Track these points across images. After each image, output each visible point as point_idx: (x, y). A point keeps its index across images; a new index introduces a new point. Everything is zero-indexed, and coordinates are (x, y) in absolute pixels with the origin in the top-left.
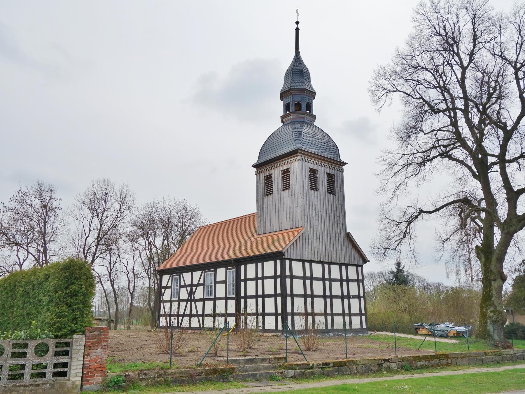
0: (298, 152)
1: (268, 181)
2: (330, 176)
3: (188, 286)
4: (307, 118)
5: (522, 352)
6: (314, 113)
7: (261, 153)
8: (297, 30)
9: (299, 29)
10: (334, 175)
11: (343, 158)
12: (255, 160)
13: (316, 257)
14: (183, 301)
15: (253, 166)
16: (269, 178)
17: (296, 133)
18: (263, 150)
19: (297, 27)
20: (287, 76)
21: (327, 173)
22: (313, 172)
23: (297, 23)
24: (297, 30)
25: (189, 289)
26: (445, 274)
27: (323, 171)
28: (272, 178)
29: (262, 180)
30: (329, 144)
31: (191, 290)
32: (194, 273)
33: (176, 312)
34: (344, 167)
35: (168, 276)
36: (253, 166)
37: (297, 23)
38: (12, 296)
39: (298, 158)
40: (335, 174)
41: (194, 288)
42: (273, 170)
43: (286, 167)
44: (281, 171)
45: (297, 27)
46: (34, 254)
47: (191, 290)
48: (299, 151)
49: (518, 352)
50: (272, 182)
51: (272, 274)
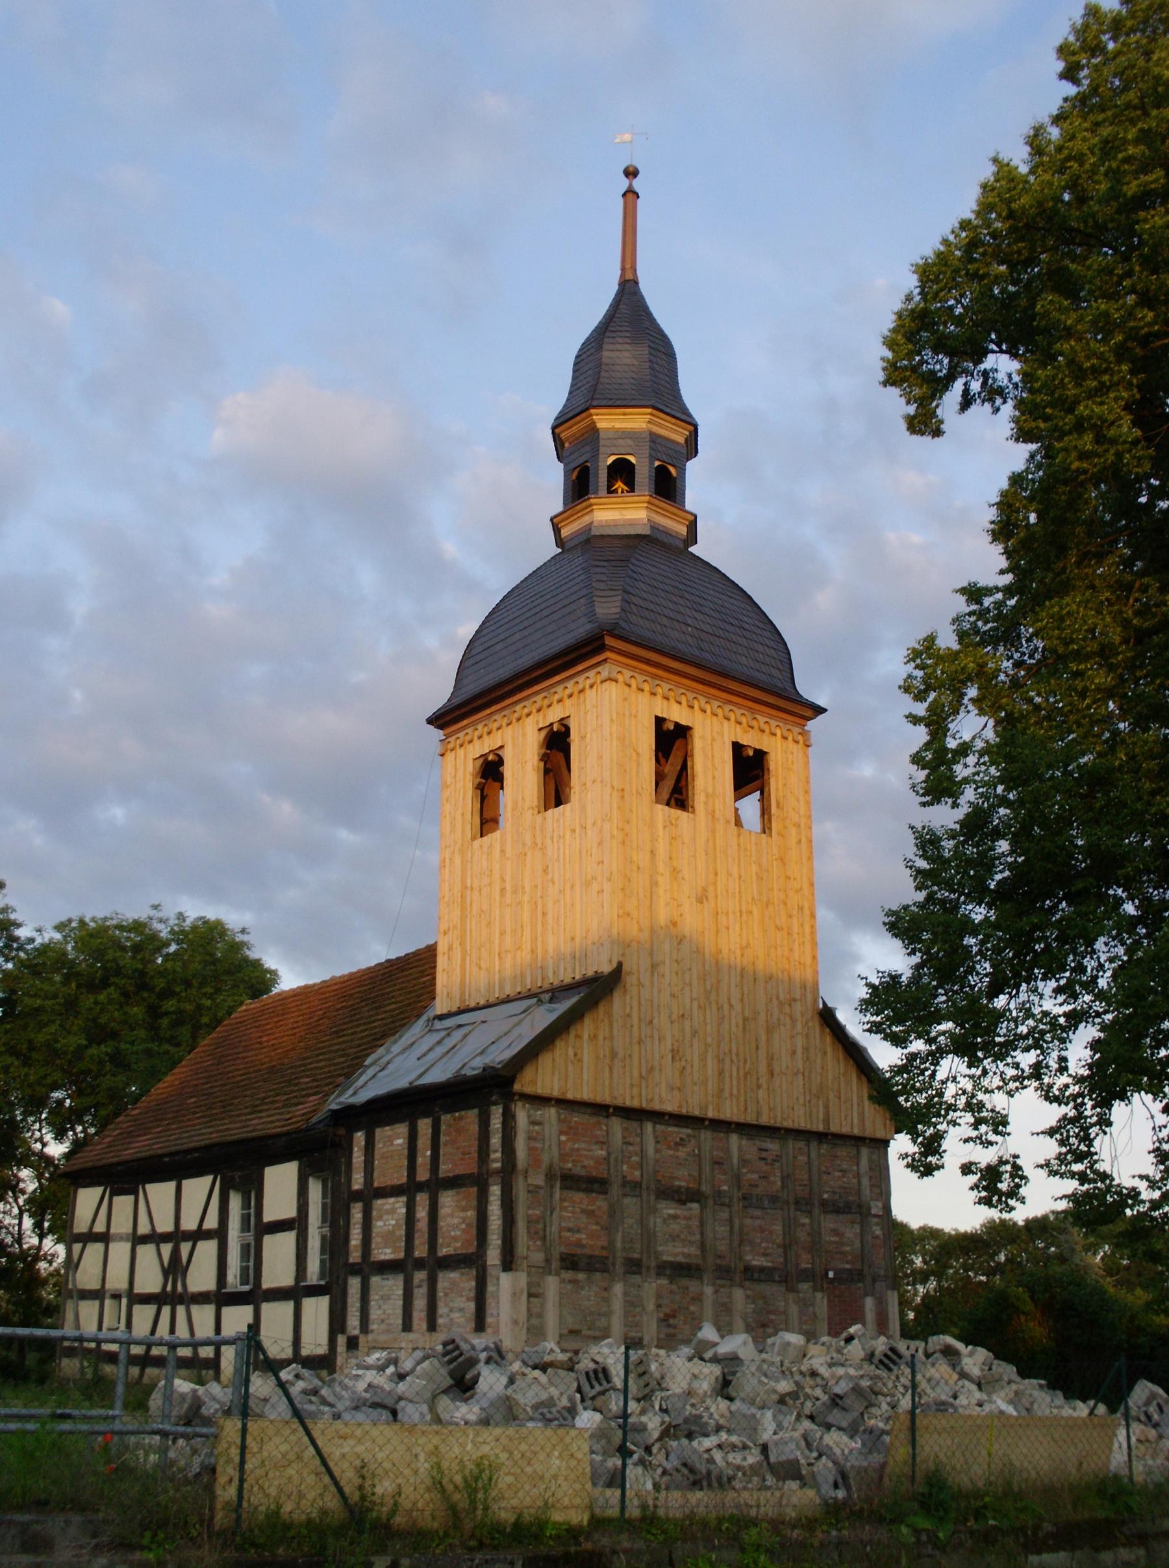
0: (602, 648)
3: (165, 1238)
7: (468, 663)
8: (630, 195)
13: (556, 1087)
14: (146, 1299)
15: (430, 721)
17: (604, 570)
18: (474, 652)
19: (631, 185)
20: (582, 364)
23: (631, 173)
24: (630, 195)
25: (166, 1249)
26: (816, 886)
30: (747, 626)
31: (176, 1253)
32: (186, 1183)
33: (446, 1279)
35: (97, 1191)
36: (430, 721)
37: (631, 173)
39: (605, 670)
41: (185, 1248)
42: (509, 731)
43: (553, 715)
44: (540, 729)
47: (176, 1253)
48: (609, 641)
51: (401, 1178)
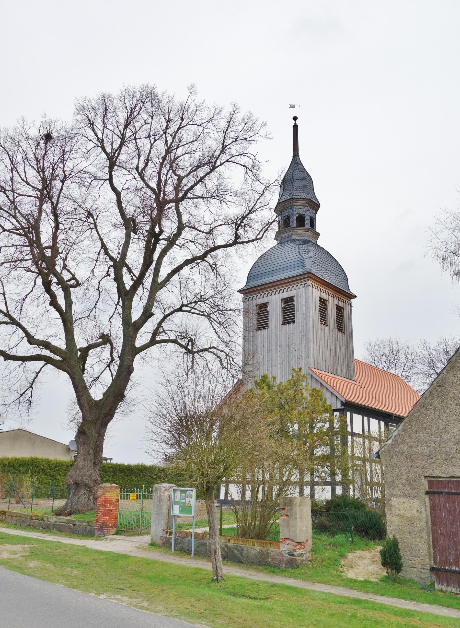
1: (261, 311)
2: (339, 309)
4: (307, 235)
5: (66, 522)
6: (318, 230)
7: (250, 276)
8: (295, 127)
9: (298, 126)
10: (343, 309)
11: (353, 289)
12: (242, 284)
16: (263, 307)
19: (295, 123)
21: (336, 305)
22: (323, 302)
23: (295, 118)
24: (295, 127)
27: (332, 303)
28: (294, 301)
29: (254, 311)
34: (353, 301)
37: (295, 118)
38: (282, 393)
40: (345, 307)
45: (295, 123)
46: (43, 365)
49: (60, 521)
50: (294, 306)
